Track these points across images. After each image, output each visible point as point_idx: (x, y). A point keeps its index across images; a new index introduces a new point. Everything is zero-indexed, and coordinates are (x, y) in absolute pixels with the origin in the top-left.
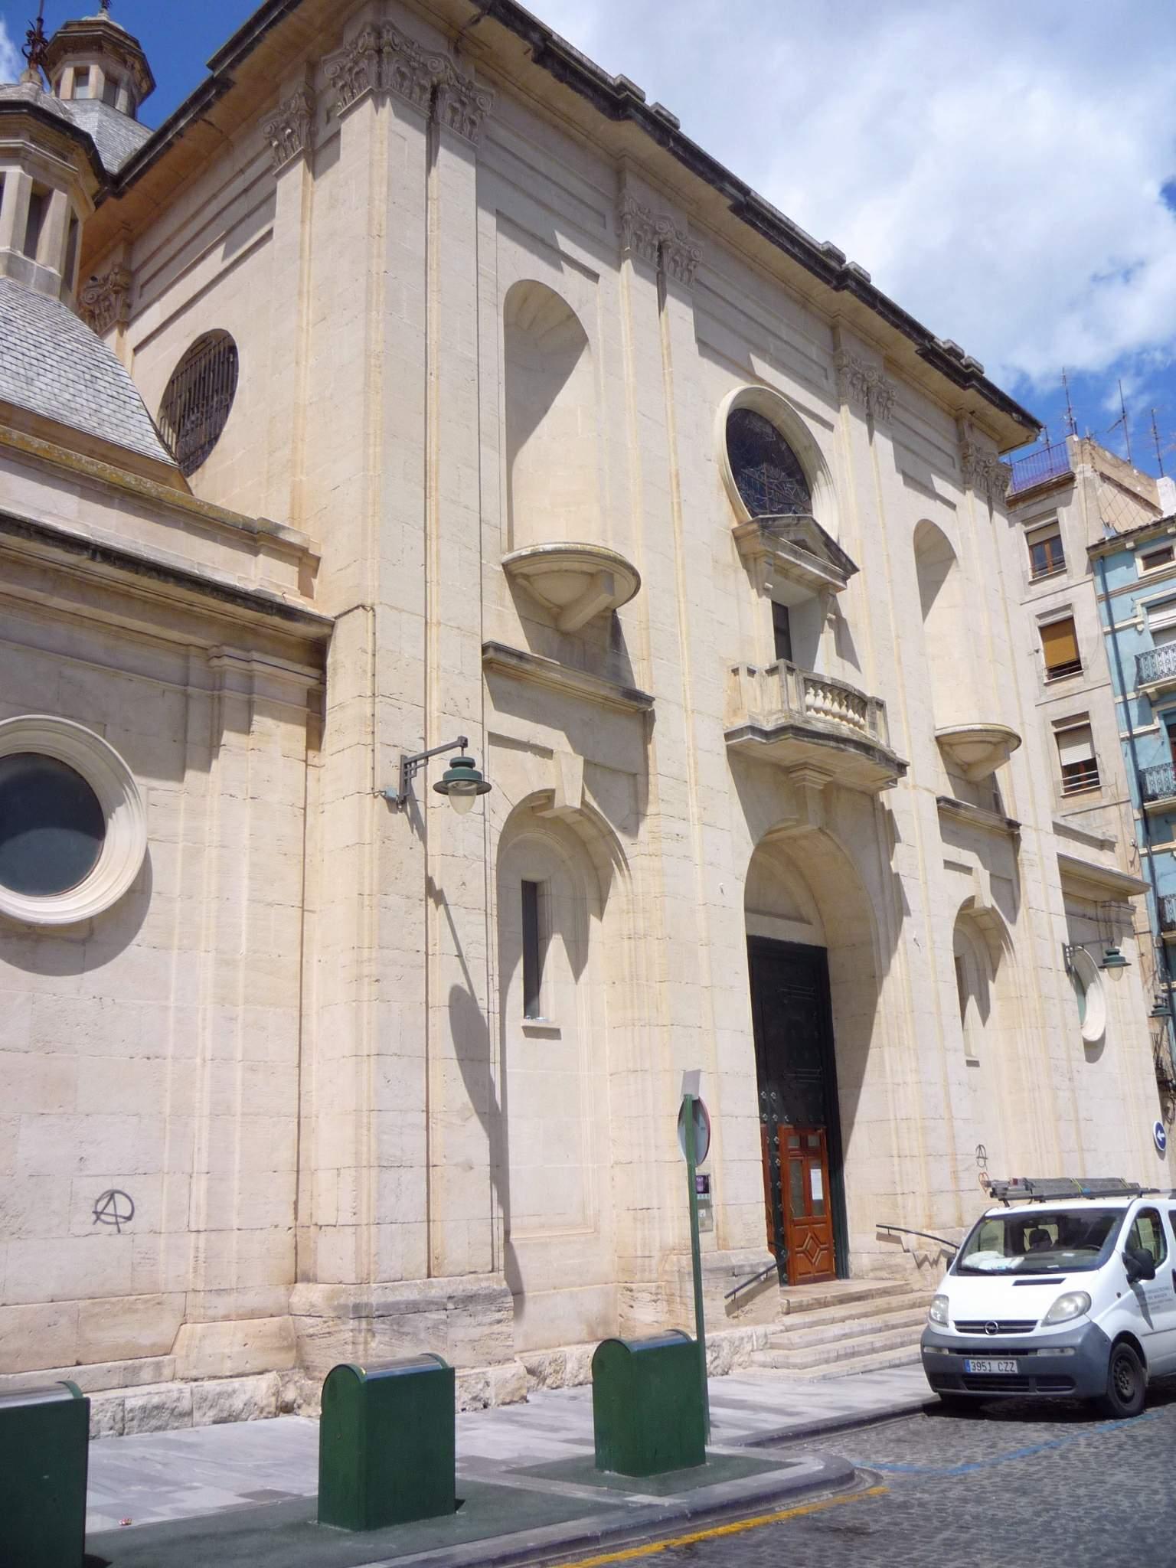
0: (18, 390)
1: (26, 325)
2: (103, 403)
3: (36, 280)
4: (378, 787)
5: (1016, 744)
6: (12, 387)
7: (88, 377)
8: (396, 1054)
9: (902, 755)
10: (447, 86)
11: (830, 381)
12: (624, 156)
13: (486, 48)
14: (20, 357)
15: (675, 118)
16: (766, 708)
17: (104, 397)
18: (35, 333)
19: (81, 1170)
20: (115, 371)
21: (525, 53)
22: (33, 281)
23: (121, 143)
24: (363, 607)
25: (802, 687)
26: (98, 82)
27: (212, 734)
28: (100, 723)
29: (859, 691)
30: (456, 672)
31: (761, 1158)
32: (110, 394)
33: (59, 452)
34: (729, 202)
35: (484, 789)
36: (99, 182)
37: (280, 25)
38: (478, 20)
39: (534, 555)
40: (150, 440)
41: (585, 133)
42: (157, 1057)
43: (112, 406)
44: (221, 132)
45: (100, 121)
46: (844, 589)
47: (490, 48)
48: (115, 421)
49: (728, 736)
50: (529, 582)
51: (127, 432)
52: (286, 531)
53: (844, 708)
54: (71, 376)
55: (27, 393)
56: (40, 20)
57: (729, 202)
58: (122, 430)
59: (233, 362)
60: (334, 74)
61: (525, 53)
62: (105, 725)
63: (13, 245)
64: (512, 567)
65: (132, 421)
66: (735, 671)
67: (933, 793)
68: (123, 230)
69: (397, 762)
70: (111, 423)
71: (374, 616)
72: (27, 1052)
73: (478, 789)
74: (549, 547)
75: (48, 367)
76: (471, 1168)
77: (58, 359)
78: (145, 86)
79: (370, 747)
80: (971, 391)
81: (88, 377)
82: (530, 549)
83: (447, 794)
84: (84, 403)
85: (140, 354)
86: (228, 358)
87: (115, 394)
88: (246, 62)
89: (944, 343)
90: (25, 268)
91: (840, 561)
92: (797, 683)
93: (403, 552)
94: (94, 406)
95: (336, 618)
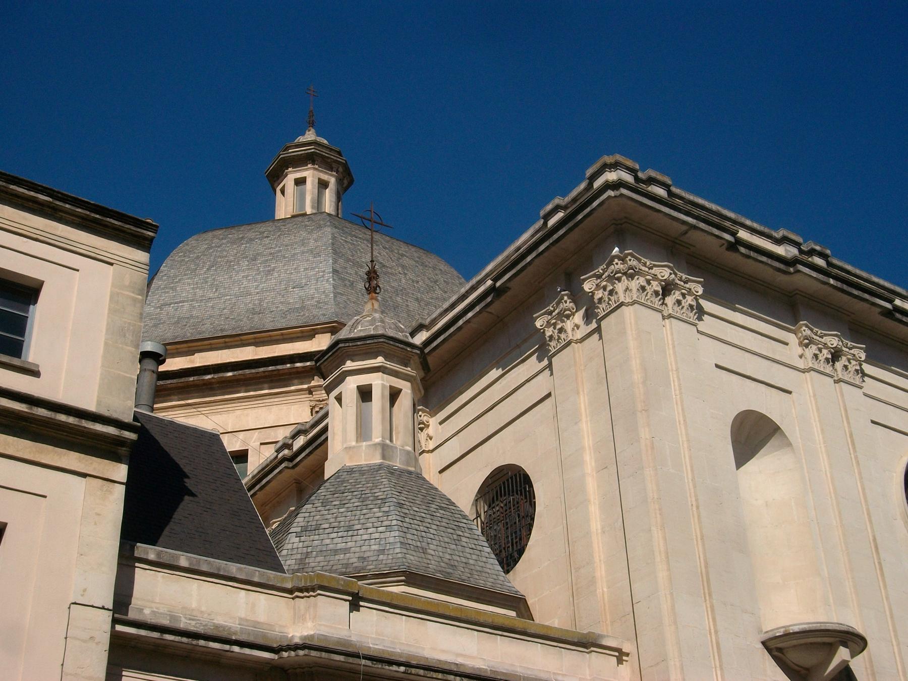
0: (420, 560)
1: (412, 505)
2: (468, 556)
7: (455, 537)
12: (796, 294)
14: (415, 532)
17: (468, 550)
22: (398, 460)
23: (349, 249)
26: (313, 188)
32: (470, 547)
33: (27, 184)
36: (425, 373)
45: (333, 234)
47: (694, 246)
48: (479, 568)
50: (783, 654)
51: (487, 575)
54: (446, 540)
55: (425, 561)
57: (879, 310)
58: (484, 574)
59: (529, 491)
60: (590, 289)
63: (383, 437)
64: (768, 644)
65: (488, 566)
70: (477, 571)
75: (432, 536)
77: (394, 484)
78: (346, 182)
81: (455, 537)
82: (782, 630)
84: (458, 559)
86: (525, 488)
87: (473, 546)
94: (464, 560)
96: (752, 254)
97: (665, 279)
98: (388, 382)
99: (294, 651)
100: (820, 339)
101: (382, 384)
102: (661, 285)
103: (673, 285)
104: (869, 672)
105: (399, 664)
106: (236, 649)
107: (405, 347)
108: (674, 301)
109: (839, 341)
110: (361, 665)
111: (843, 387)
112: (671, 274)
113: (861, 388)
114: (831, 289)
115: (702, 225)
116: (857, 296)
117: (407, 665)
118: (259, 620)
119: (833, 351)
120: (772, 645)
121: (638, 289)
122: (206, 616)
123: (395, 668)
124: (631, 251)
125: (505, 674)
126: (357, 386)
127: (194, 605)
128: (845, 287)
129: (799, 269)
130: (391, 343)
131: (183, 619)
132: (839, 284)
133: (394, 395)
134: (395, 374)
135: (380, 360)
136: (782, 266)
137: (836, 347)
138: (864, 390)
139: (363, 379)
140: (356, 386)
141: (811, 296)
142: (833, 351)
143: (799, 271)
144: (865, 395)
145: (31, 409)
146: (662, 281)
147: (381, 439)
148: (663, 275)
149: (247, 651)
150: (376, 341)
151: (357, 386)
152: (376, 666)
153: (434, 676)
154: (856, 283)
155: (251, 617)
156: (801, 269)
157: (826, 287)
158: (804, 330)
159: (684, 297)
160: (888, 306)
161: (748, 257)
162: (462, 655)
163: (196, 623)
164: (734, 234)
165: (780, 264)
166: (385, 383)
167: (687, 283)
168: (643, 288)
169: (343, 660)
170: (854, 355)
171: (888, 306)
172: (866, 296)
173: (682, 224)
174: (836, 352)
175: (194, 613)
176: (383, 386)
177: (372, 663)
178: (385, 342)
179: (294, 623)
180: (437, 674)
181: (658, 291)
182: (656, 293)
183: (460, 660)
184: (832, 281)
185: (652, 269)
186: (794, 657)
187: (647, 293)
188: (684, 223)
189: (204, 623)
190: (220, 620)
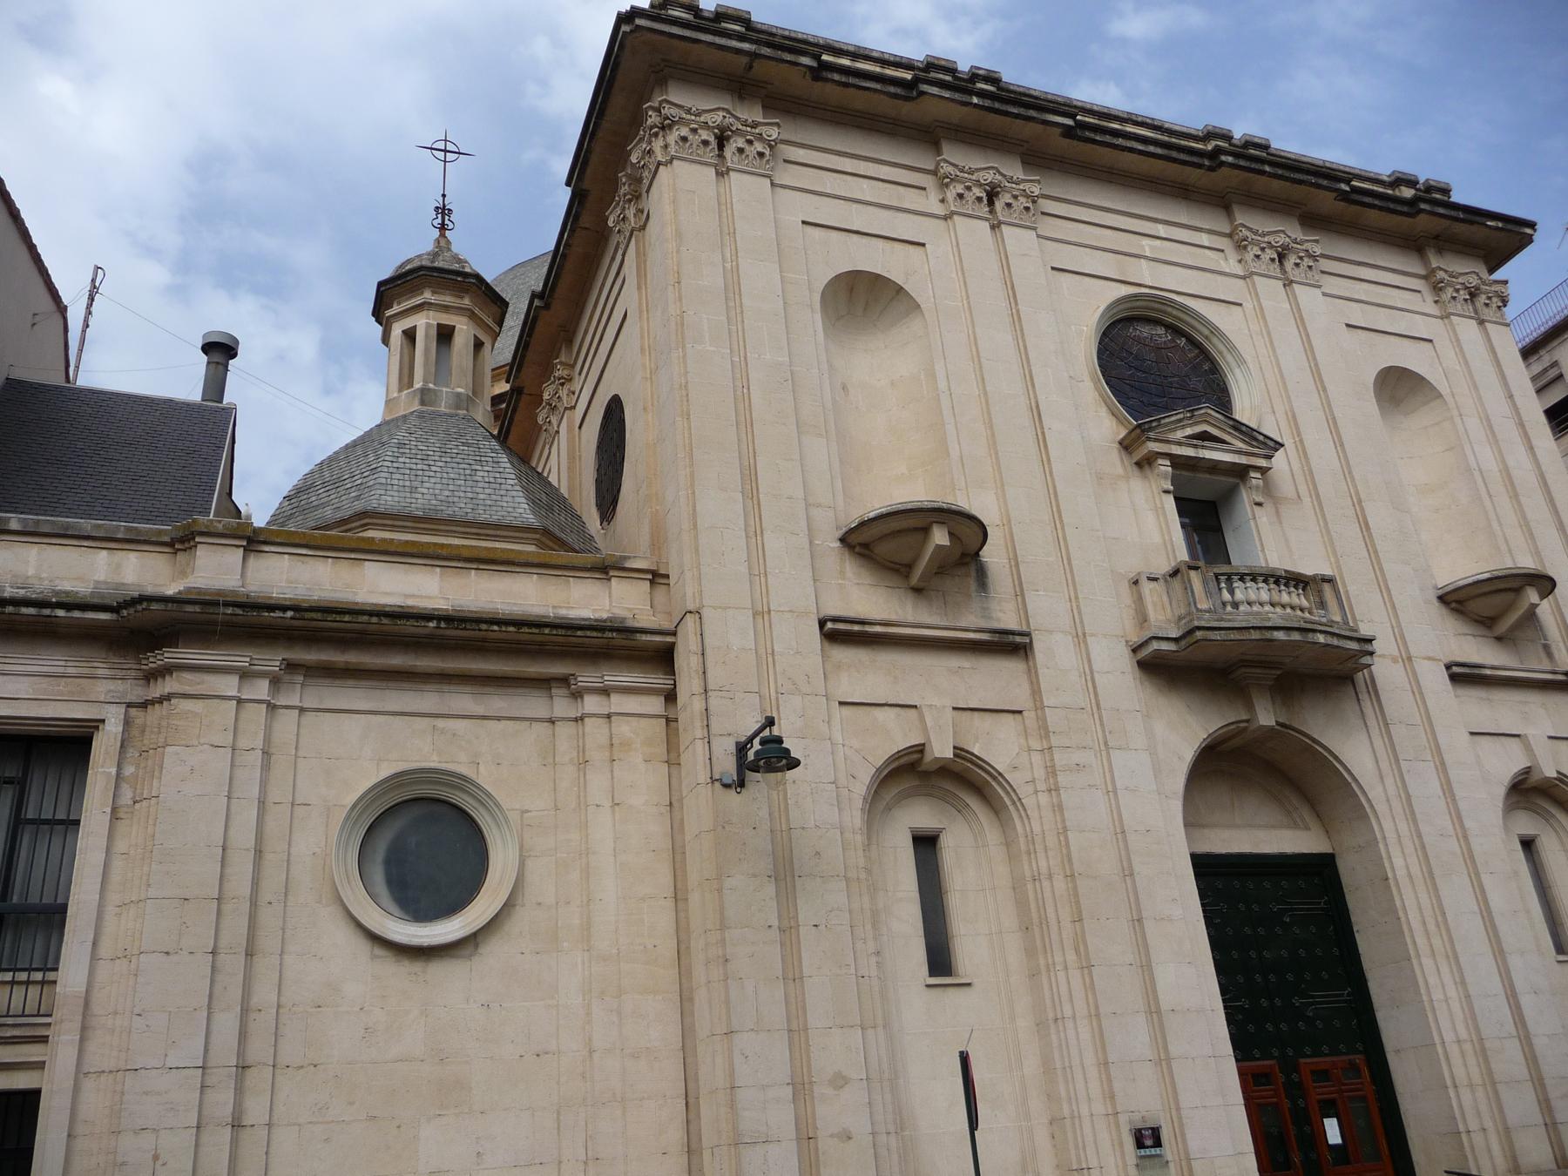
3: (446, 402)
4: (717, 776)
5: (1550, 587)
6: (396, 499)
8: (752, 1030)
9: (1365, 630)
10: (730, 133)
11: (1231, 261)
13: (769, 86)
15: (996, 72)
16: (1176, 614)
18: (426, 448)
19: (478, 1164)
20: (495, 460)
21: (804, 76)
24: (690, 612)
25: (1213, 584)
27: (578, 753)
28: (473, 762)
29: (1286, 571)
30: (792, 653)
31: (1243, 1102)
34: (1059, 131)
35: (794, 764)
37: (600, 134)
38: (751, 67)
39: (862, 524)
40: (522, 511)
41: (891, 121)
42: (547, 1053)
43: (487, 491)
44: (597, 232)
46: (1271, 468)
49: (1134, 651)
52: (632, 560)
53: (1294, 595)
56: (444, 196)
57: (1059, 131)
61: (804, 76)
62: (478, 764)
66: (1136, 582)
67: (1440, 660)
68: (562, 333)
69: (733, 749)
71: (700, 618)
72: (422, 1061)
73: (787, 764)
74: (872, 515)
76: (850, 1138)
79: (707, 740)
80: (1422, 216)
83: (759, 772)
85: (583, 428)
88: (589, 171)
89: (1389, 176)
90: (436, 395)
91: (1256, 439)
92: (1205, 582)
93: (723, 555)
95: (676, 627)
96: (852, 80)
97: (718, 125)
98: (434, 319)
99: (126, 609)
100: (970, 176)
101: (427, 323)
102: (985, 190)
103: (1001, 187)
104: (1013, 563)
105: (284, 609)
106: (61, 613)
107: (454, 277)
108: (1252, 256)
109: (995, 174)
110: (219, 614)
111: (1454, 322)
112: (724, 117)
113: (1319, 287)
114: (977, 111)
115: (766, 51)
116: (1017, 114)
117: (296, 608)
118: (126, 581)
119: (987, 188)
120: (854, 539)
121: (676, 142)
122: (46, 582)
123: (278, 614)
124: (778, 120)
125: (476, 612)
126: (403, 331)
127: (31, 572)
128: (997, 105)
129: (922, 89)
130: (435, 274)
131: (9, 589)
132: (987, 103)
133: (445, 335)
134: (446, 309)
135: (427, 295)
136: (899, 91)
137: (991, 182)
138: (1323, 289)
139: (407, 323)
140: (400, 331)
141: (958, 126)
142: (987, 188)
143: (923, 93)
144: (1325, 294)
145: (1289, 636)
146: (714, 127)
147: (421, 384)
148: (985, 178)
149: (77, 614)
150: (416, 275)
151: (403, 331)
152: (249, 614)
153: (338, 619)
154: (1064, 105)
155: (118, 579)
156: (925, 90)
157: (965, 109)
158: (1241, 231)
159: (969, 188)
160: (1070, 122)
161: (846, 85)
162: (413, 596)
163: (26, 592)
164: (817, 58)
165: (896, 89)
166: (431, 322)
167: (755, 128)
168: (961, 196)
169: (198, 610)
170: (1307, 251)
171: (1070, 122)
172: (1032, 113)
173: (736, 54)
174: (993, 189)
175: (30, 581)
176: (428, 326)
177: (244, 611)
178: (426, 275)
179: (173, 581)
180: (342, 616)
181: (982, 198)
182: (1273, 260)
183: (410, 602)
184: (975, 100)
185: (700, 116)
186: (884, 550)
187: (692, 144)
188: (738, 51)
189: (38, 591)
190: (66, 586)
